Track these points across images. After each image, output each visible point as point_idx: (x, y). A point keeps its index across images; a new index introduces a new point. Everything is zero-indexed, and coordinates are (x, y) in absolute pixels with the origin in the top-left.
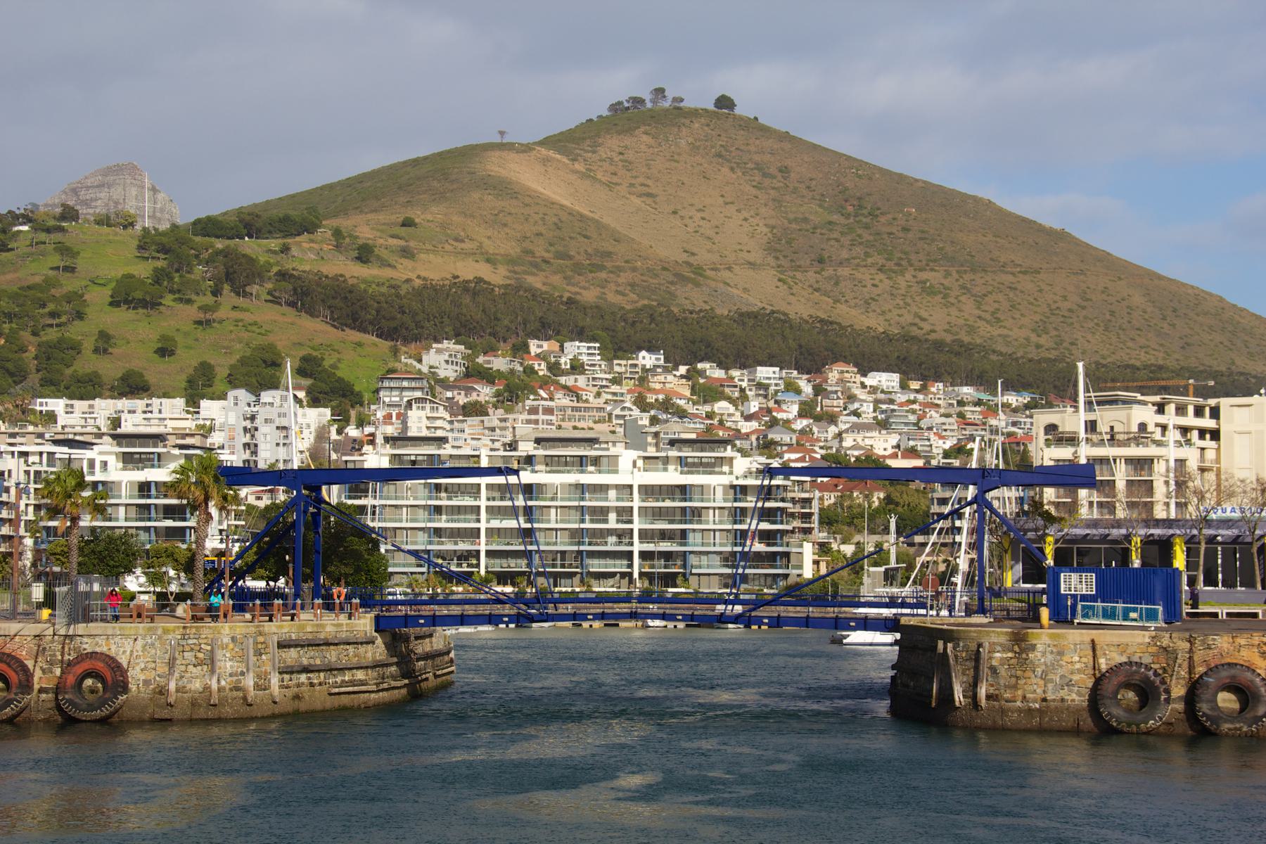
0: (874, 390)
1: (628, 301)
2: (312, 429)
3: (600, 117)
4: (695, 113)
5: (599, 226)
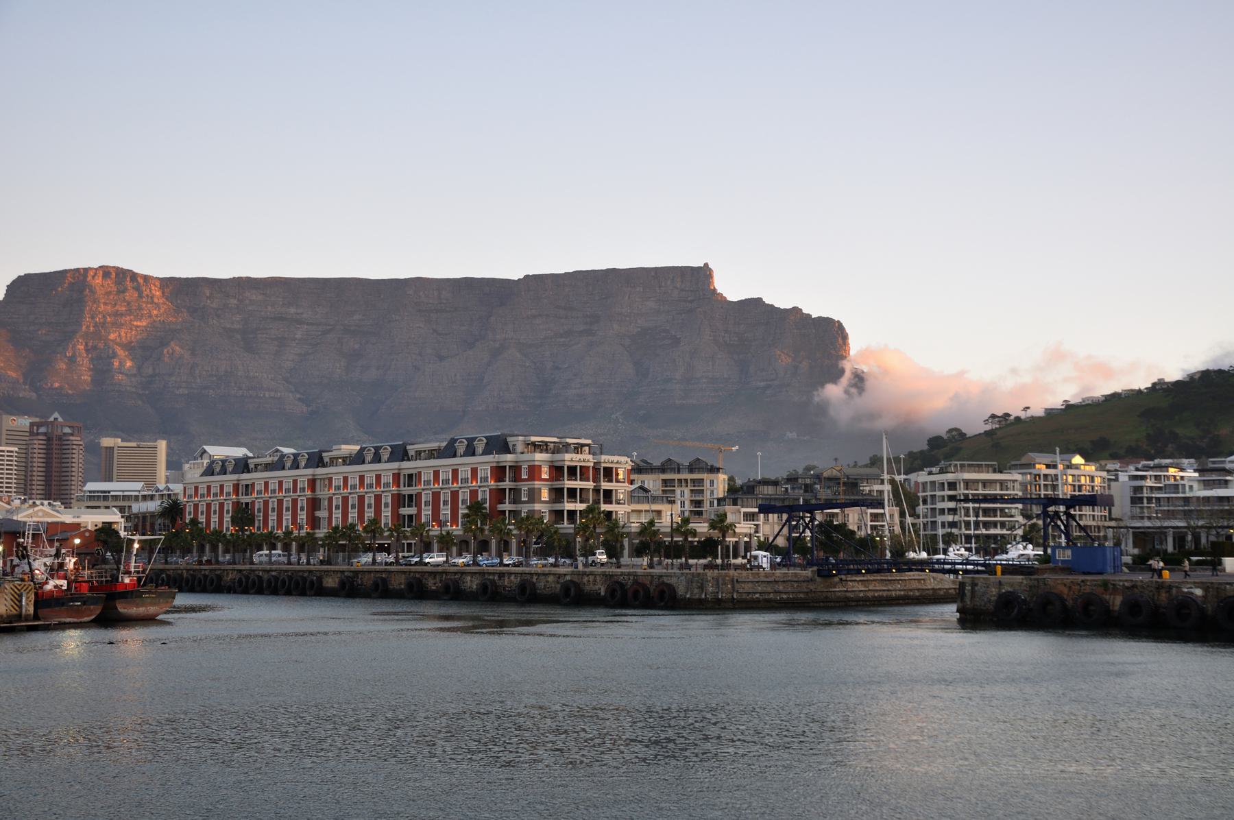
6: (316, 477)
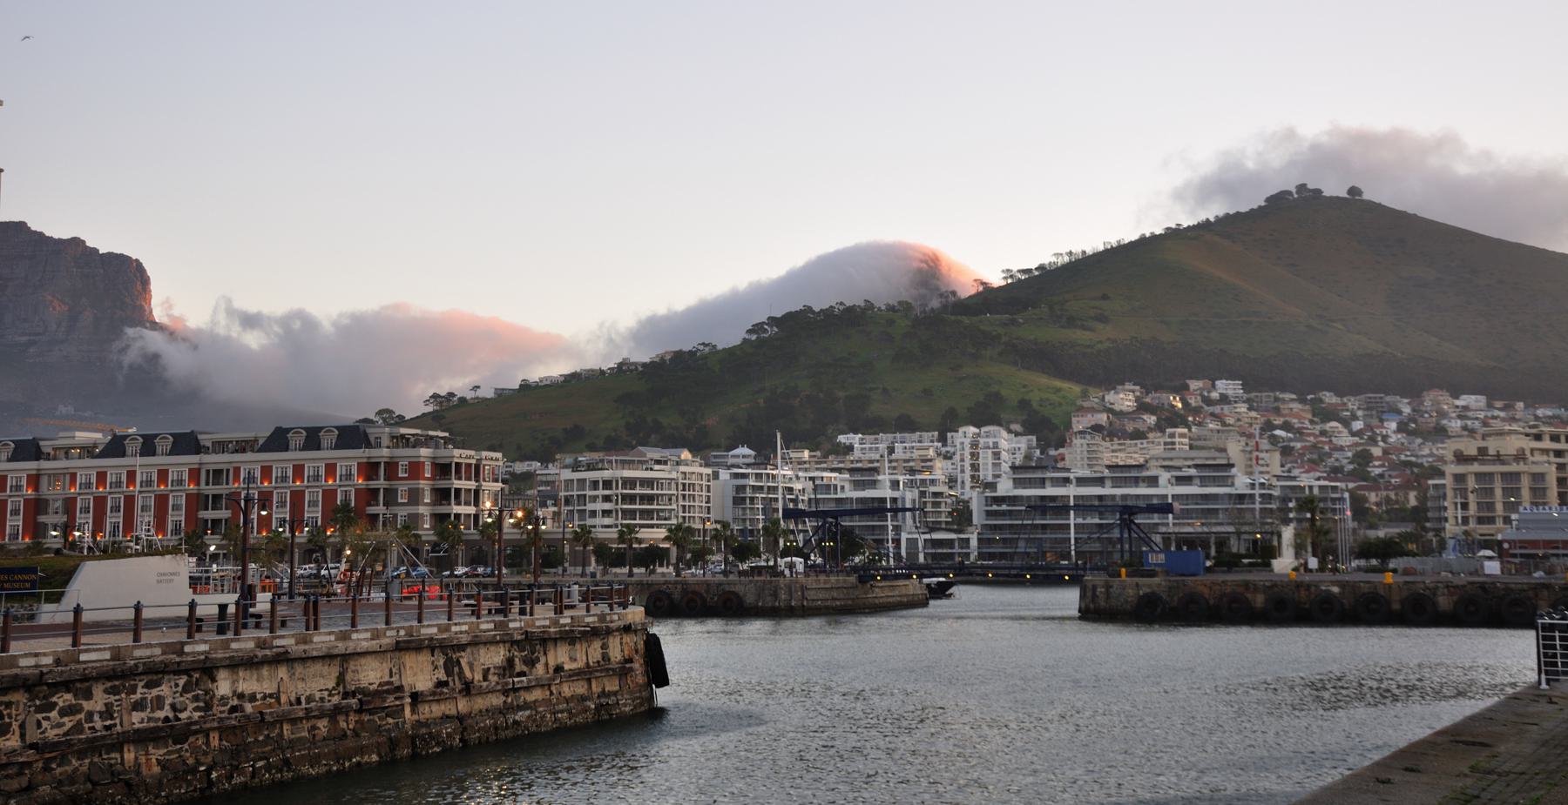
3: (1260, 207)
6: (43, 472)
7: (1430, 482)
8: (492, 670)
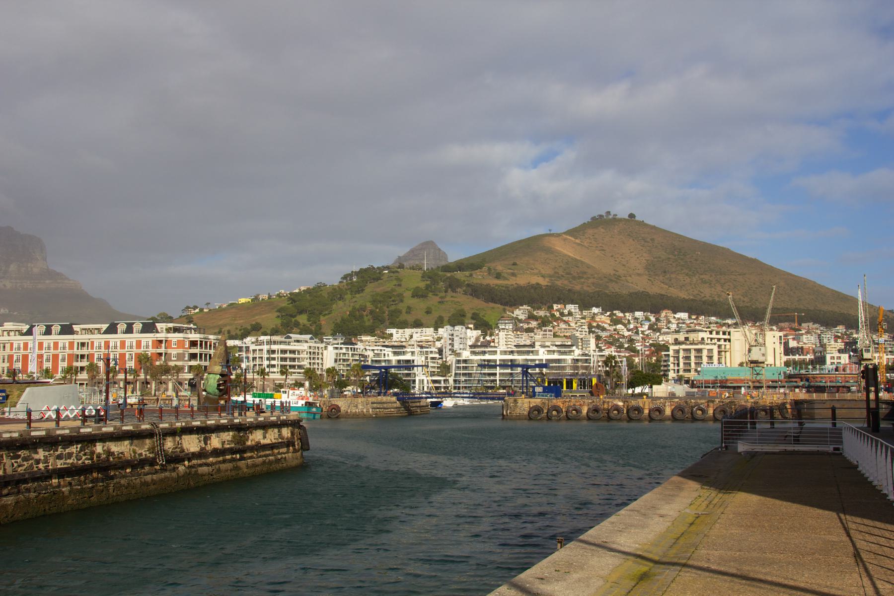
0: (679, 319)
1: (591, 290)
2: (474, 337)
3: (588, 222)
4: (621, 220)
5: (582, 262)
7: (663, 353)
8: (226, 443)
